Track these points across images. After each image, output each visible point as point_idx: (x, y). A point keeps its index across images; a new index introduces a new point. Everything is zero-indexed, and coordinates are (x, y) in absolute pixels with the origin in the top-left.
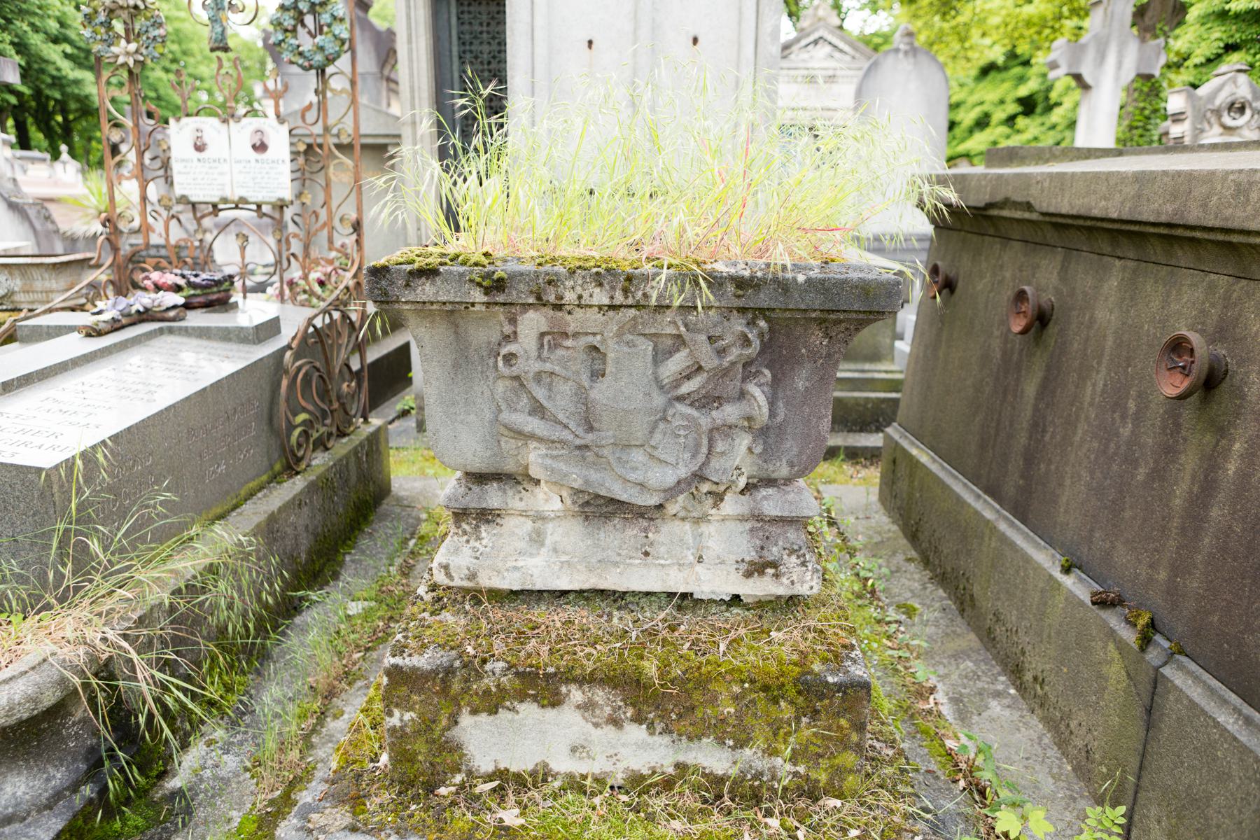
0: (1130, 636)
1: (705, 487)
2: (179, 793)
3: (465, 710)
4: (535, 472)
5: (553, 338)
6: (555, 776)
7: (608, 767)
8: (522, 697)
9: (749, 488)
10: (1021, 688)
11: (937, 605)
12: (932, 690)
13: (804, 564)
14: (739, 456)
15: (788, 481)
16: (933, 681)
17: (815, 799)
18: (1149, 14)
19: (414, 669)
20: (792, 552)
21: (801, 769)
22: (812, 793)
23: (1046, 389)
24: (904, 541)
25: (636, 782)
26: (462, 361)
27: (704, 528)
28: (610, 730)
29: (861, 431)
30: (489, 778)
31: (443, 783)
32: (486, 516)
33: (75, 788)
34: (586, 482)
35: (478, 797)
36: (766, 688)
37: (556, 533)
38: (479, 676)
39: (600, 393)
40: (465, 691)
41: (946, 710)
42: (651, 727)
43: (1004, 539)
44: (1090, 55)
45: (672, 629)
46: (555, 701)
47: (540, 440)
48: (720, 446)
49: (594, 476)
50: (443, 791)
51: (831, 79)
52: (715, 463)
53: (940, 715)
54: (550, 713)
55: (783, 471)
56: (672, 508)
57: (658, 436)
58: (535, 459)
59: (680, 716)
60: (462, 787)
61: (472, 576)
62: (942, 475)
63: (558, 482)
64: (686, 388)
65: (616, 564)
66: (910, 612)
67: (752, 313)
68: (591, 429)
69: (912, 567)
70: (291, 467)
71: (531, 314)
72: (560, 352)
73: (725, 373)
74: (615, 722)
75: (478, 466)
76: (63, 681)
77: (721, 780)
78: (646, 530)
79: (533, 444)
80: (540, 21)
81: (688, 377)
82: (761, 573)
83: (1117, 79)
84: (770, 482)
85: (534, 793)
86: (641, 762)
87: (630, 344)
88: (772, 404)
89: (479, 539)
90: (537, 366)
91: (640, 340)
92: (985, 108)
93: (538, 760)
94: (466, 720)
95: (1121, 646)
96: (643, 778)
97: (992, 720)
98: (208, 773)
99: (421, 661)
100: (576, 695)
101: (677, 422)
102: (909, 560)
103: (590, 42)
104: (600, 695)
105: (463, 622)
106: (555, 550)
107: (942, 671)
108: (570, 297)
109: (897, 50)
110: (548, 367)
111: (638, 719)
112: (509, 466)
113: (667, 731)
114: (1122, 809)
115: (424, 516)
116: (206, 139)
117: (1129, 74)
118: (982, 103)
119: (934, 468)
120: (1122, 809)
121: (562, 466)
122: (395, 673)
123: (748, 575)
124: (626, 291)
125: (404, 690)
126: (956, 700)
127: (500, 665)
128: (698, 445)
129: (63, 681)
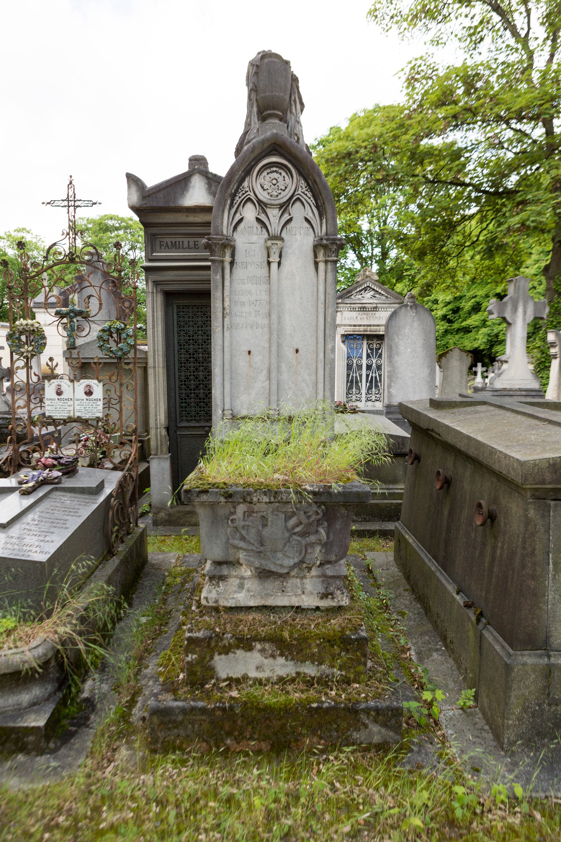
0: (474, 618)
1: (304, 566)
2: (87, 700)
3: (216, 654)
4: (241, 561)
5: (249, 513)
6: (250, 679)
7: (270, 675)
8: (238, 647)
9: (321, 565)
10: (446, 646)
11: (416, 612)
12: (409, 649)
13: (343, 593)
14: (317, 553)
15: (336, 562)
16: (410, 645)
17: (349, 685)
18: (551, 270)
19: (197, 638)
20: (338, 589)
21: (343, 673)
22: (348, 682)
23: (451, 514)
24: (404, 581)
25: (281, 680)
26: (215, 521)
27: (305, 581)
28: (271, 660)
29: (389, 521)
30: (225, 680)
31: (207, 683)
32: (222, 578)
33: (55, 693)
34: (261, 565)
35: (221, 688)
36: (329, 641)
37: (248, 584)
38: (222, 639)
39: (266, 532)
40: (216, 646)
41: (413, 658)
42: (287, 659)
43: (439, 580)
44: (509, 308)
45: (294, 620)
46: (250, 649)
47: (244, 549)
48: (309, 551)
49: (264, 562)
50: (207, 686)
51: (375, 309)
52: (308, 557)
53: (411, 659)
54: (249, 654)
55: (334, 558)
56: (293, 574)
57: (287, 547)
58: (242, 556)
59: (297, 653)
60: (214, 685)
61: (216, 601)
62: (417, 549)
63: (250, 564)
64: (297, 530)
65: (272, 595)
66: (402, 614)
67: (319, 504)
68: (262, 545)
69: (406, 593)
70: (111, 552)
71: (241, 505)
72: (251, 518)
73: (310, 524)
74: (273, 656)
75: (219, 558)
76: (53, 648)
77: (313, 678)
78: (283, 582)
79: (241, 551)
80: (227, 344)
81: (297, 526)
82: (327, 597)
83: (524, 320)
84: (329, 562)
85: (244, 685)
86: (282, 672)
87: (277, 515)
88: (328, 534)
89: (219, 587)
90: (243, 523)
91: (280, 514)
92: (477, 299)
93: (243, 672)
94: (217, 657)
95: (472, 622)
96: (284, 678)
97: (433, 661)
98: (97, 691)
99: (200, 635)
100: (258, 646)
101: (294, 542)
102: (405, 590)
103: (249, 352)
104: (267, 646)
105: (213, 620)
106: (248, 591)
107: (414, 641)
108: (255, 499)
109: (406, 306)
110: (247, 523)
111: (282, 655)
112: (231, 559)
113: (292, 659)
114: (474, 690)
115: (167, 574)
116: (62, 389)
117: (530, 317)
118: (476, 296)
119: (414, 545)
120: (474, 690)
121: (252, 559)
122: (190, 639)
123: (322, 598)
124: (275, 497)
125: (193, 646)
126: (418, 653)
127: (230, 635)
128: (301, 551)
129: (53, 648)
